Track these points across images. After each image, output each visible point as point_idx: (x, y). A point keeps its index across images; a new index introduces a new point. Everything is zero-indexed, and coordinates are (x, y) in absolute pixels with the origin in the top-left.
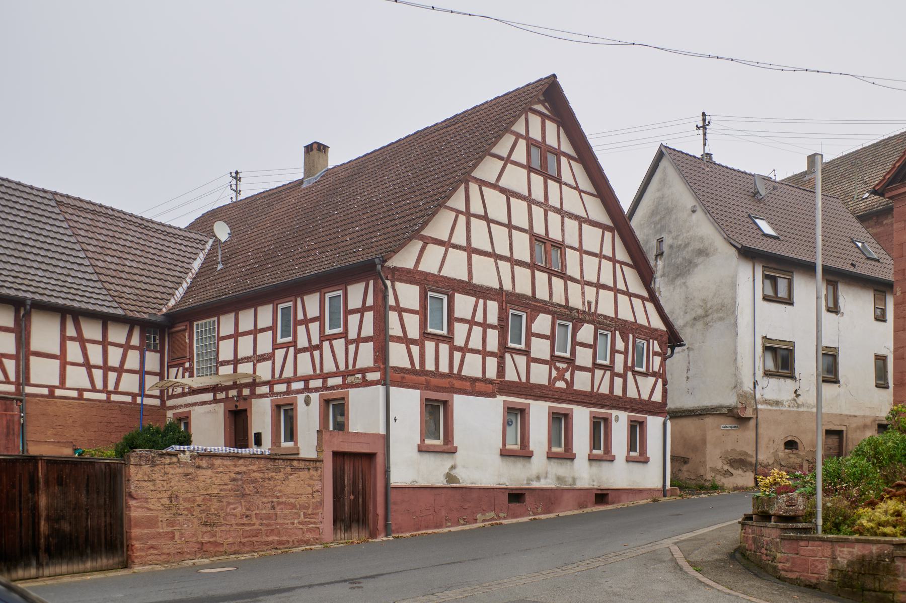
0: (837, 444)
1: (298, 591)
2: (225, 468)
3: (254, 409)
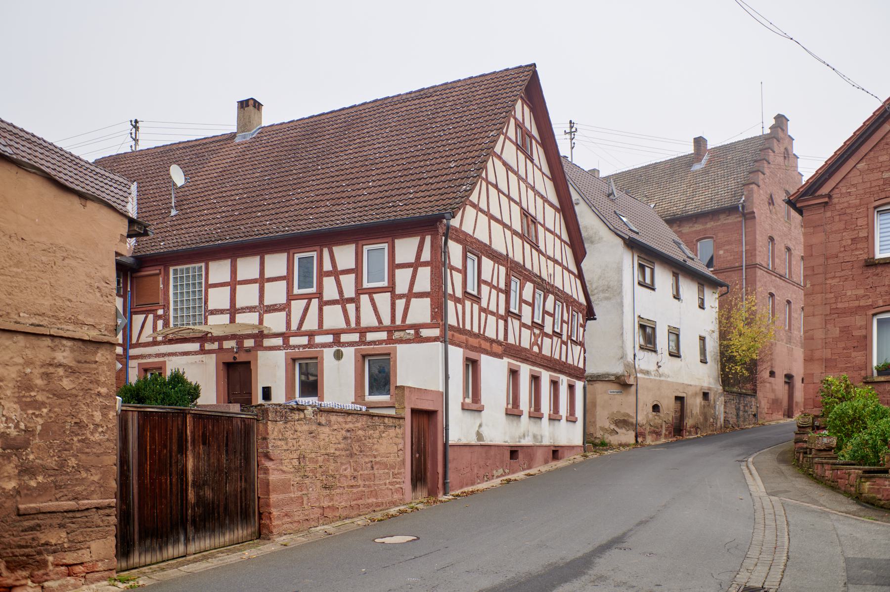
0: (679, 408)
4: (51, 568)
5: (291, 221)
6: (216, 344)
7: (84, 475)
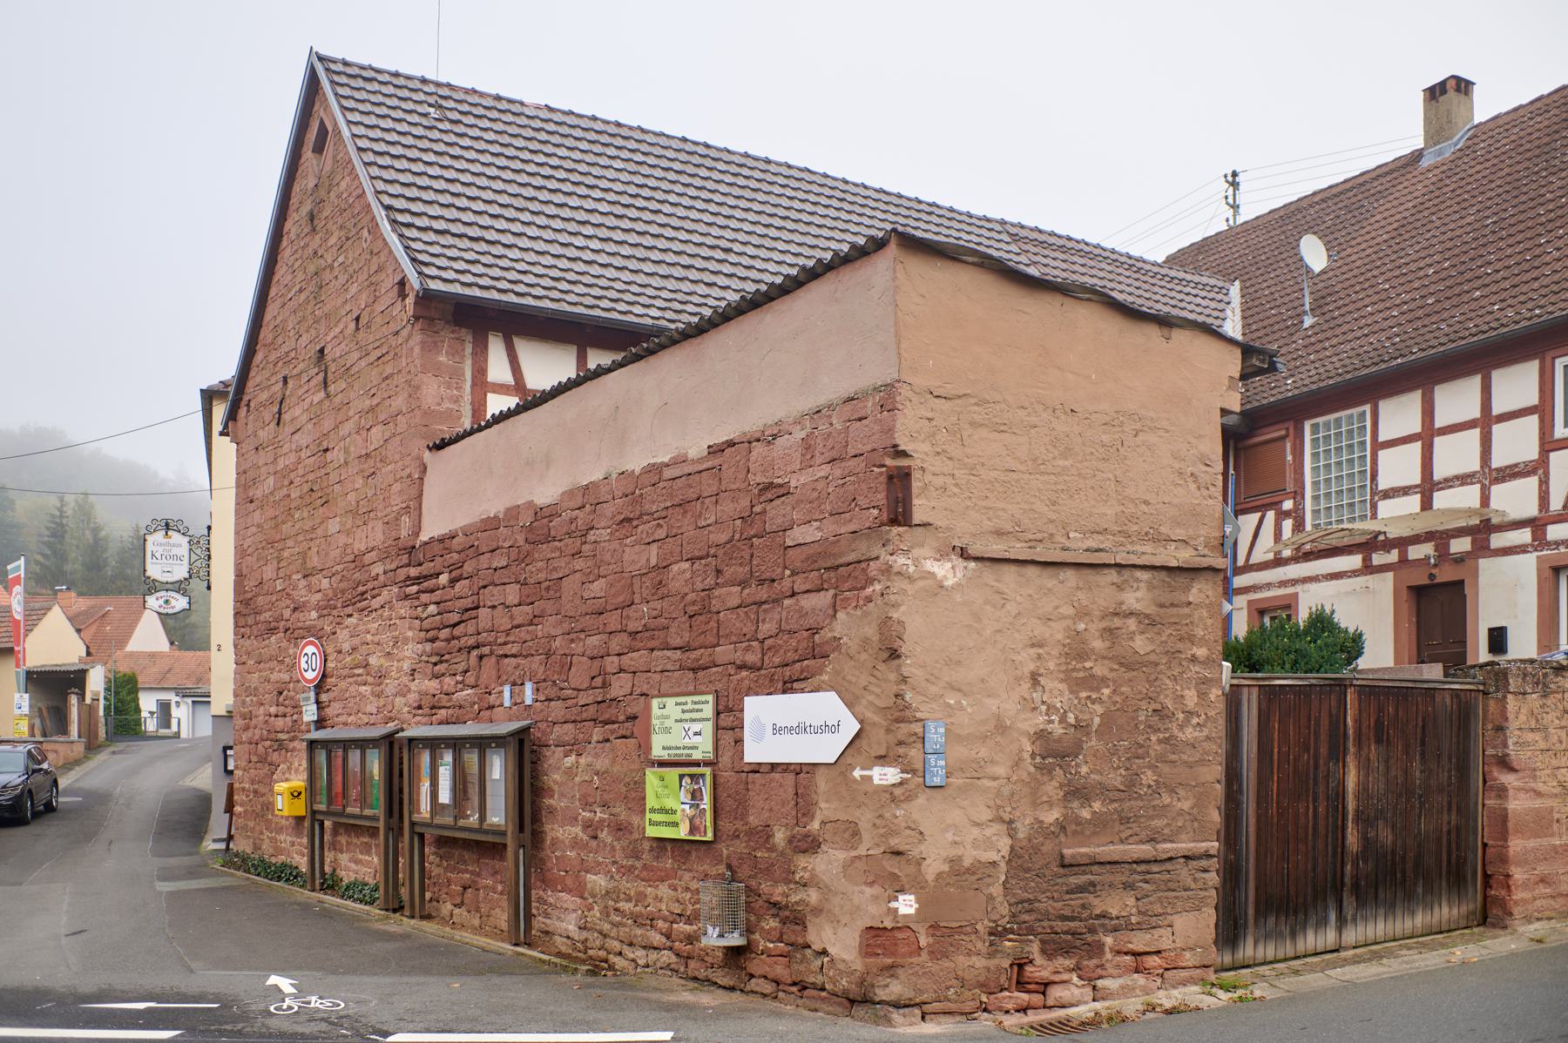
3: (1483, 579)
4: (1109, 956)
5: (1545, 296)
6: (1395, 552)
7: (1166, 799)
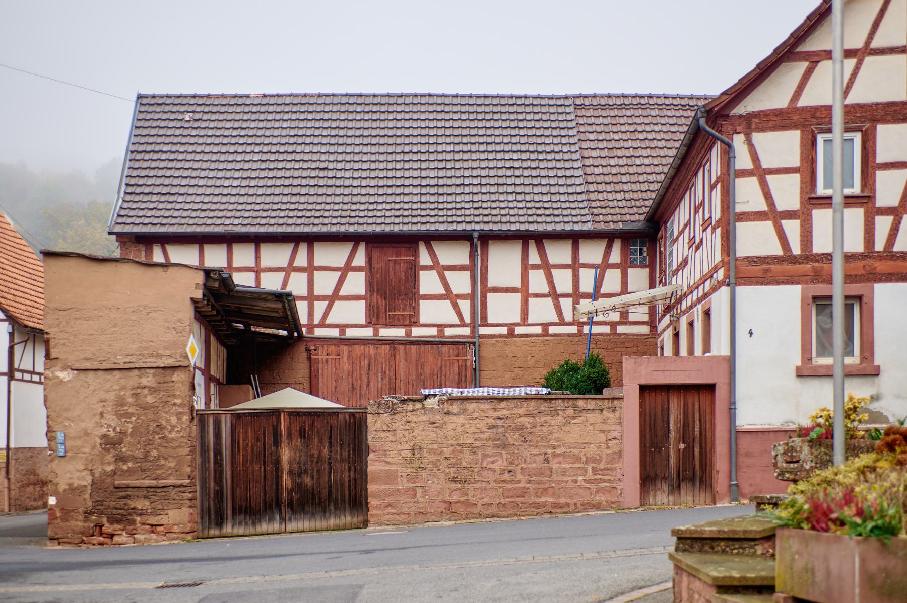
1: (377, 552)
2: (482, 413)
